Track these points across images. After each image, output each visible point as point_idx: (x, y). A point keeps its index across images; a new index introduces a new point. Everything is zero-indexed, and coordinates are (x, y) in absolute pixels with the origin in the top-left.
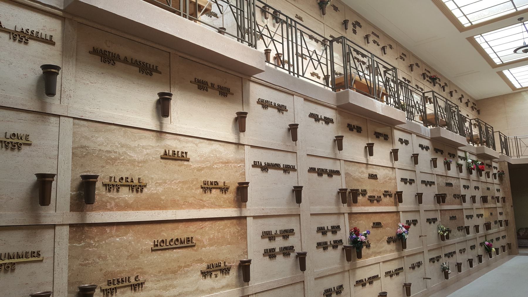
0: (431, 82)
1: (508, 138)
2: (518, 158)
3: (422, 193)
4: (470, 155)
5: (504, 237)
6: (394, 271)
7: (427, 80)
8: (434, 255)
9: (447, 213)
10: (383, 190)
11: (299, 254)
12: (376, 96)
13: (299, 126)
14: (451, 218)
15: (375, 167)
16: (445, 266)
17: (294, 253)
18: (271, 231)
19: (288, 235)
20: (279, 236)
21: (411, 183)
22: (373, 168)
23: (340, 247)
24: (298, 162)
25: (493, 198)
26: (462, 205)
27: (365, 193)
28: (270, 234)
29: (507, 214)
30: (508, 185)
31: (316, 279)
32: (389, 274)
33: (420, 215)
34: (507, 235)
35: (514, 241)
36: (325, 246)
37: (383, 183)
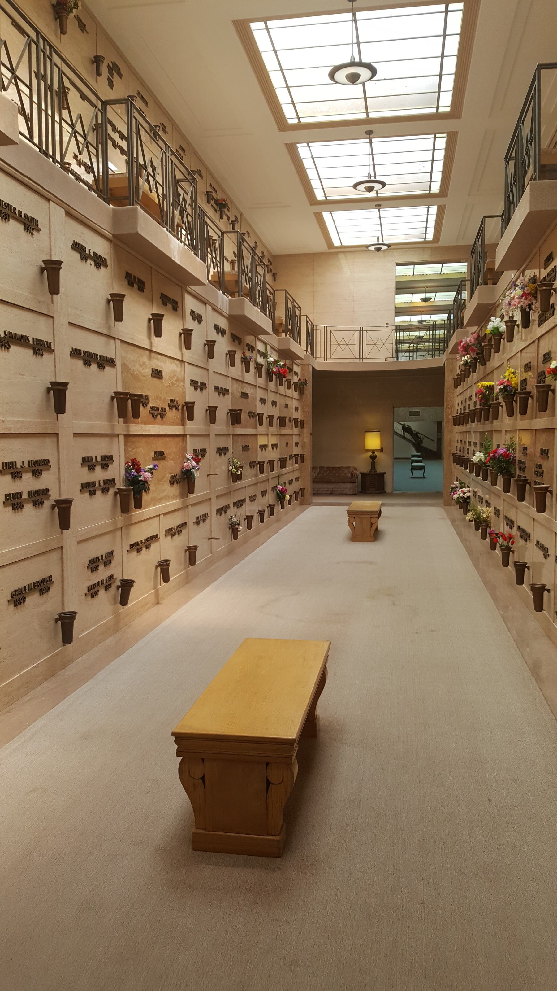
0: (216, 211)
1: (315, 328)
2: (325, 361)
3: (217, 407)
4: (272, 350)
5: (297, 479)
6: (175, 528)
7: (212, 206)
8: (222, 503)
9: (240, 440)
10: (169, 399)
11: (58, 503)
12: (170, 228)
13: (63, 266)
14: (243, 448)
15: (160, 356)
16: (235, 519)
17: (49, 501)
18: (15, 462)
19: (41, 470)
20: (27, 471)
21: (202, 390)
22: (158, 359)
23: (112, 491)
24: (55, 335)
25: (290, 420)
26: (256, 428)
27: (146, 401)
28: (14, 467)
29: (303, 446)
30: (309, 401)
31: (79, 542)
32: (170, 532)
33: (209, 442)
34: (301, 477)
35: (308, 486)
36: (92, 489)
37: (170, 386)
